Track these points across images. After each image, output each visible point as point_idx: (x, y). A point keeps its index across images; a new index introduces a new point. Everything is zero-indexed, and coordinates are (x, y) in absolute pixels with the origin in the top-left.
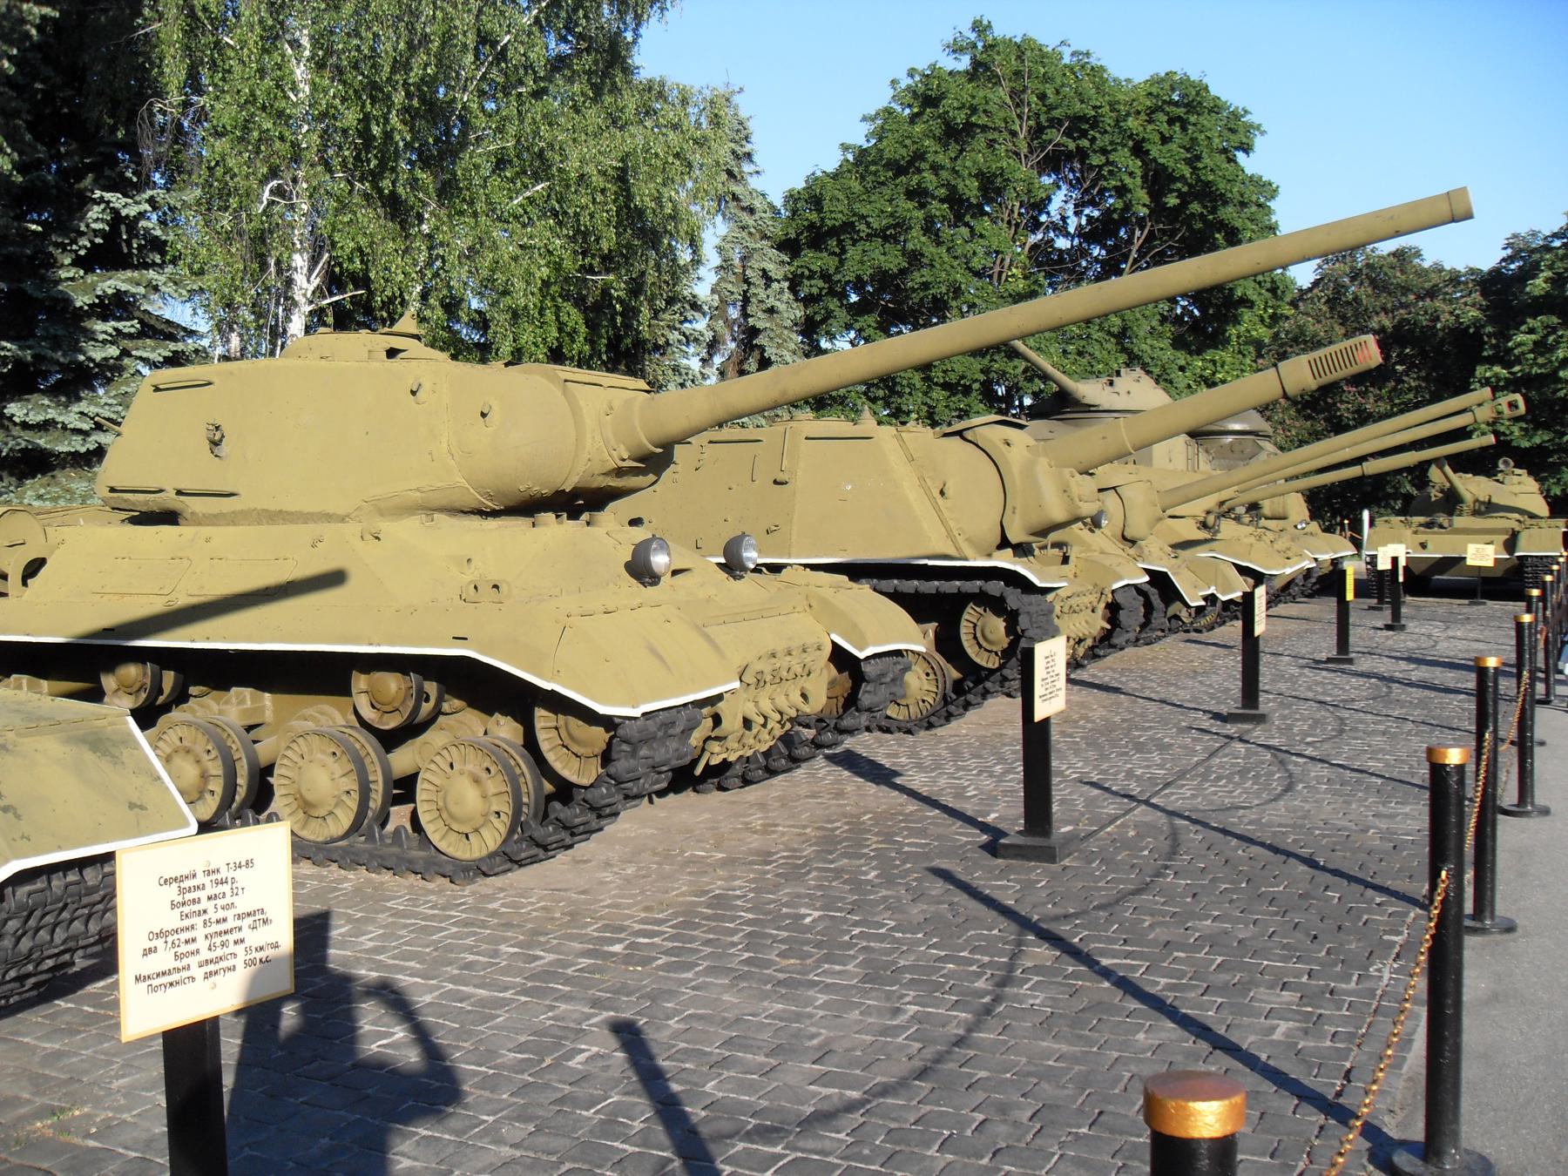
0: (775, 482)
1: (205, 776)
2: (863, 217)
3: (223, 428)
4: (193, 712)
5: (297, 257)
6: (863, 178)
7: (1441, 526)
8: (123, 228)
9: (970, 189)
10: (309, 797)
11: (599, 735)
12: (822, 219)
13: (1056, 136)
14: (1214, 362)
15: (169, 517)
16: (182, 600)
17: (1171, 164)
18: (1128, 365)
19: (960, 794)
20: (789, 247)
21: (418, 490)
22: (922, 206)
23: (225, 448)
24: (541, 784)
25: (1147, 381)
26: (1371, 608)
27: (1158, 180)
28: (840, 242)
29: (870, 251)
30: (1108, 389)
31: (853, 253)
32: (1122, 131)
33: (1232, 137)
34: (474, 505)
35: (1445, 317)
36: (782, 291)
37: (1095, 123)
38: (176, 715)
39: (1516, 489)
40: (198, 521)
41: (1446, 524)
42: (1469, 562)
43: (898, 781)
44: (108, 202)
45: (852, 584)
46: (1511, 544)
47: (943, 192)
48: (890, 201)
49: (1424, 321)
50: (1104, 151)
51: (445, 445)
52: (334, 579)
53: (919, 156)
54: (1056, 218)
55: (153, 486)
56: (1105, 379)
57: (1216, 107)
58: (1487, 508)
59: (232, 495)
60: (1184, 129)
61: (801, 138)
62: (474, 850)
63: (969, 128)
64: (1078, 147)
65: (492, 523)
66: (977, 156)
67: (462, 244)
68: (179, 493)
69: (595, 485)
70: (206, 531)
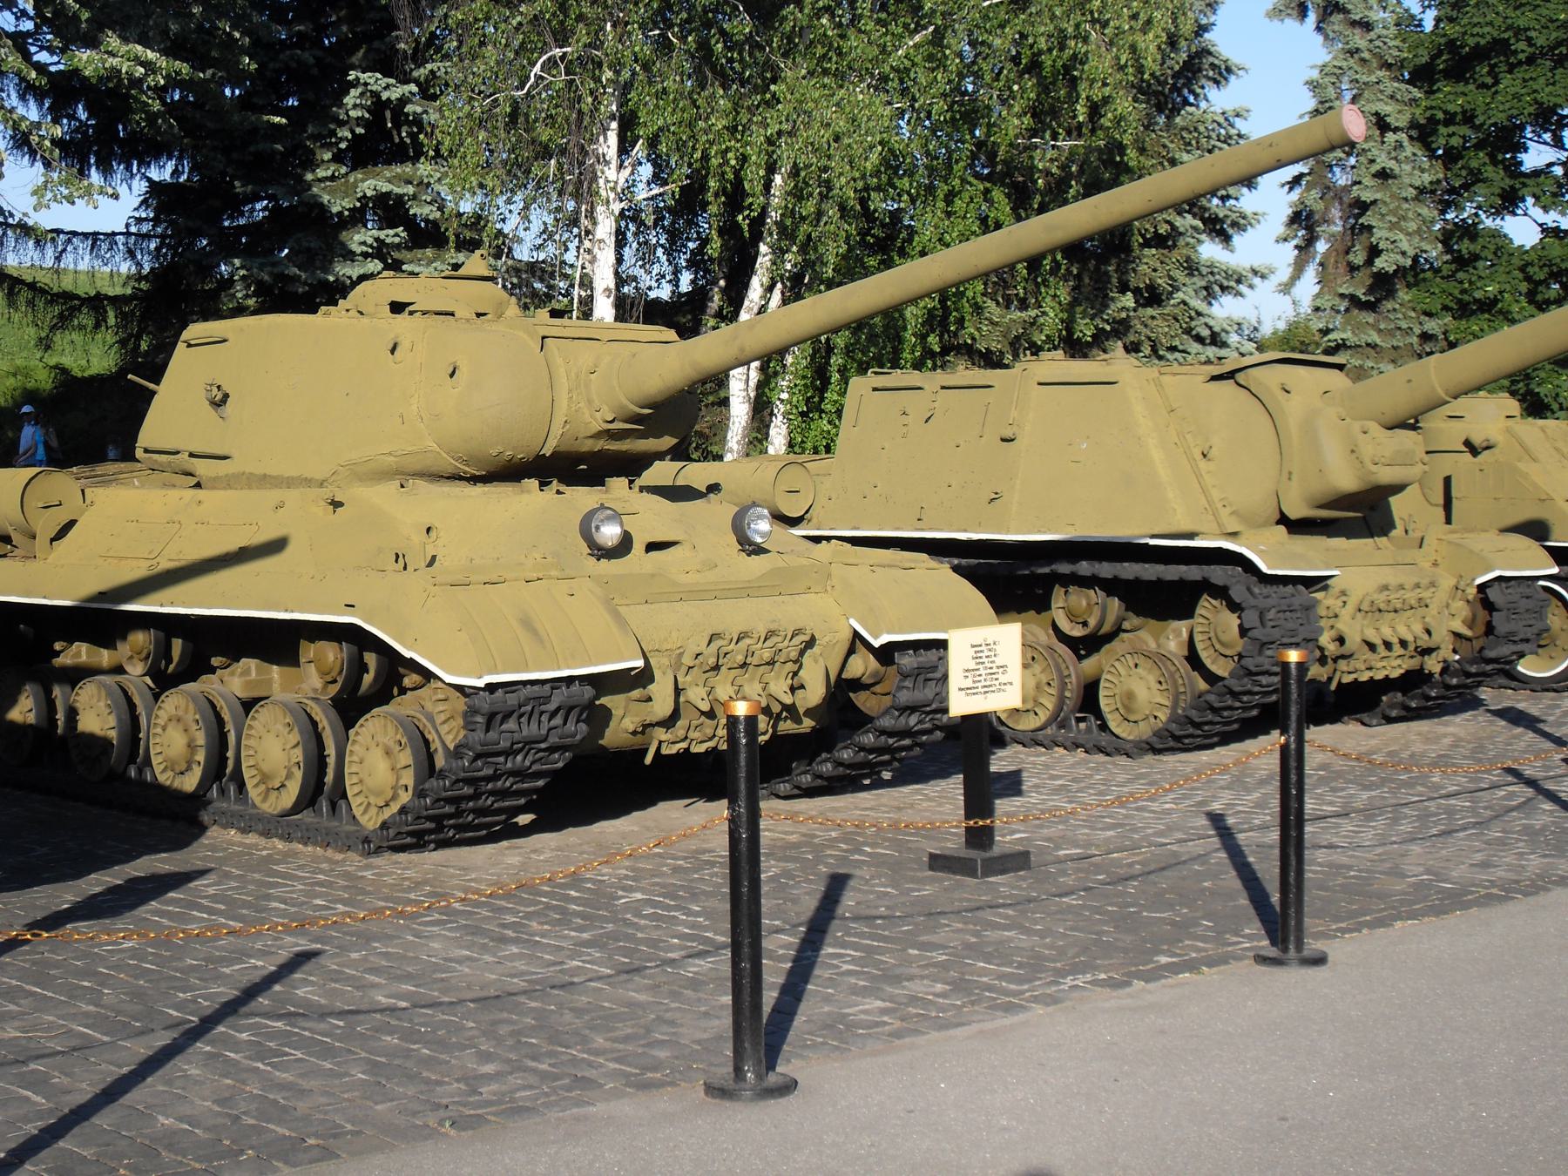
1: (191, 747)
8: (388, 114)
16: (165, 564)
28: (1492, 72)
34: (451, 470)
36: (1399, 146)
44: (366, 84)
51: (414, 407)
52: (276, 546)
59: (225, 458)
65: (480, 489)
68: (192, 455)
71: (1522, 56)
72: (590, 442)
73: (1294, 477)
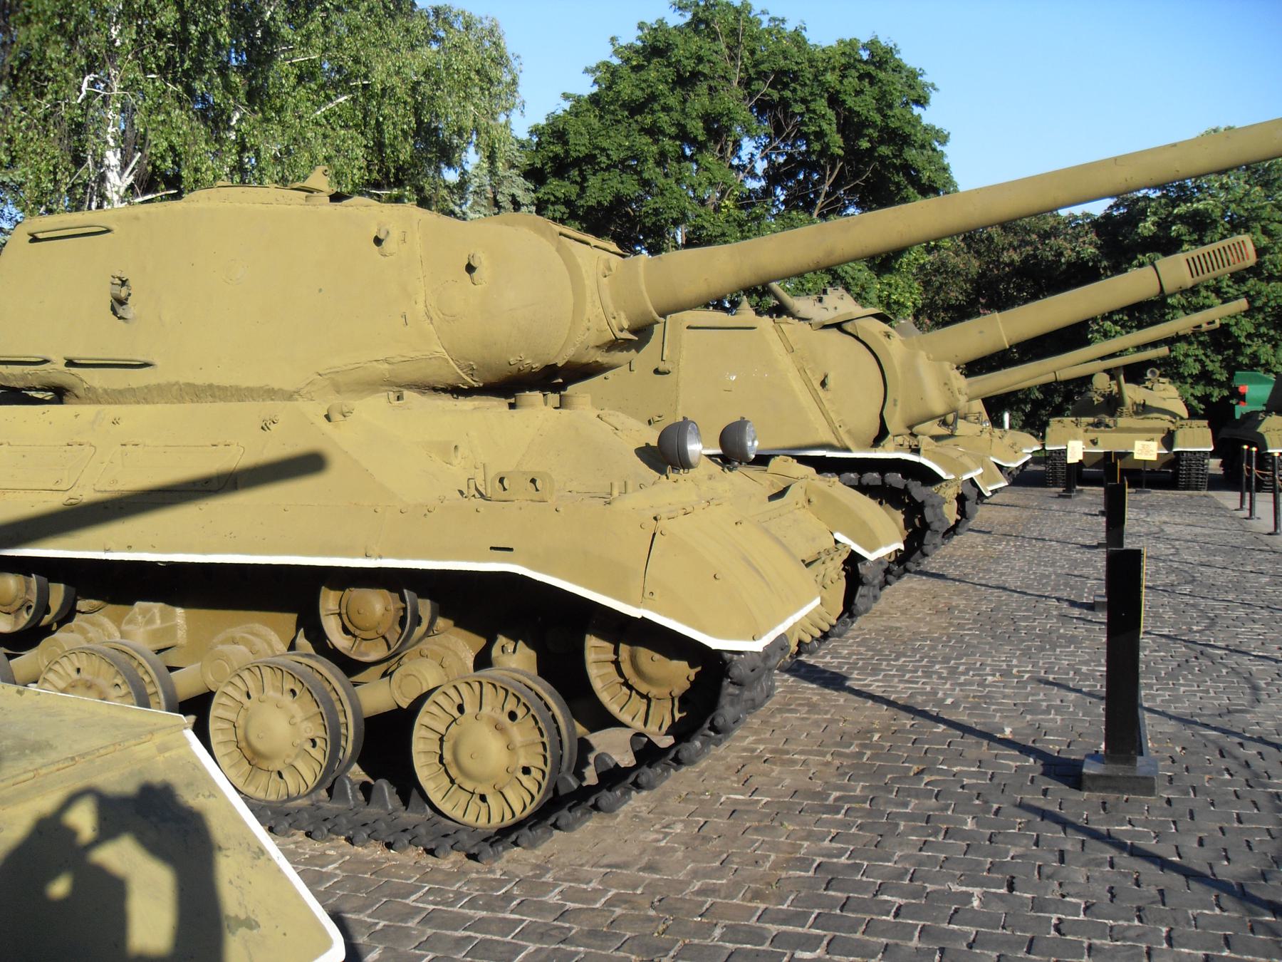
0: (657, 371)
2: (603, 150)
3: (131, 283)
4: (83, 631)
5: (109, 154)
6: (601, 117)
7: (1107, 426)
9: (696, 128)
10: (260, 746)
11: (680, 673)
12: (567, 152)
13: (763, 87)
14: (890, 285)
15: (60, 394)
16: (87, 494)
17: (865, 112)
18: (831, 285)
19: (940, 703)
20: (534, 175)
21: (386, 361)
22: (656, 141)
23: (130, 311)
24: (574, 727)
25: (848, 299)
26: (1060, 496)
27: (851, 125)
28: (581, 172)
29: (601, 179)
30: (818, 305)
31: (594, 182)
32: (821, 84)
33: (913, 92)
35: (1067, 253)
37: (795, 79)
38: (61, 636)
39: (1164, 394)
40: (93, 397)
41: (1111, 423)
42: (1136, 457)
43: (848, 683)
45: (818, 477)
46: (1168, 440)
47: (673, 130)
48: (627, 137)
49: (1050, 256)
50: (804, 101)
51: (421, 306)
53: (653, 98)
54: (745, 158)
55: (37, 355)
56: (815, 297)
57: (899, 68)
58: (1143, 409)
60: (871, 84)
61: (549, 80)
62: (497, 815)
63: (695, 75)
64: (782, 98)
66: (700, 101)
67: (275, 149)
68: (70, 363)
69: (585, 360)
70: (112, 410)
71: (603, 166)
72: (592, 352)
73: (899, 404)
